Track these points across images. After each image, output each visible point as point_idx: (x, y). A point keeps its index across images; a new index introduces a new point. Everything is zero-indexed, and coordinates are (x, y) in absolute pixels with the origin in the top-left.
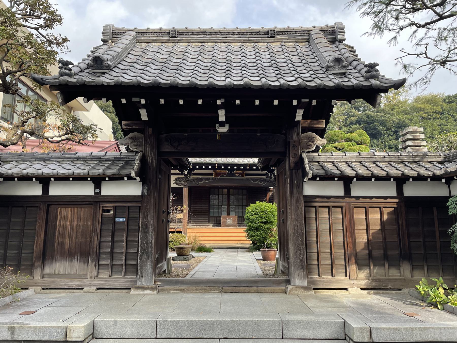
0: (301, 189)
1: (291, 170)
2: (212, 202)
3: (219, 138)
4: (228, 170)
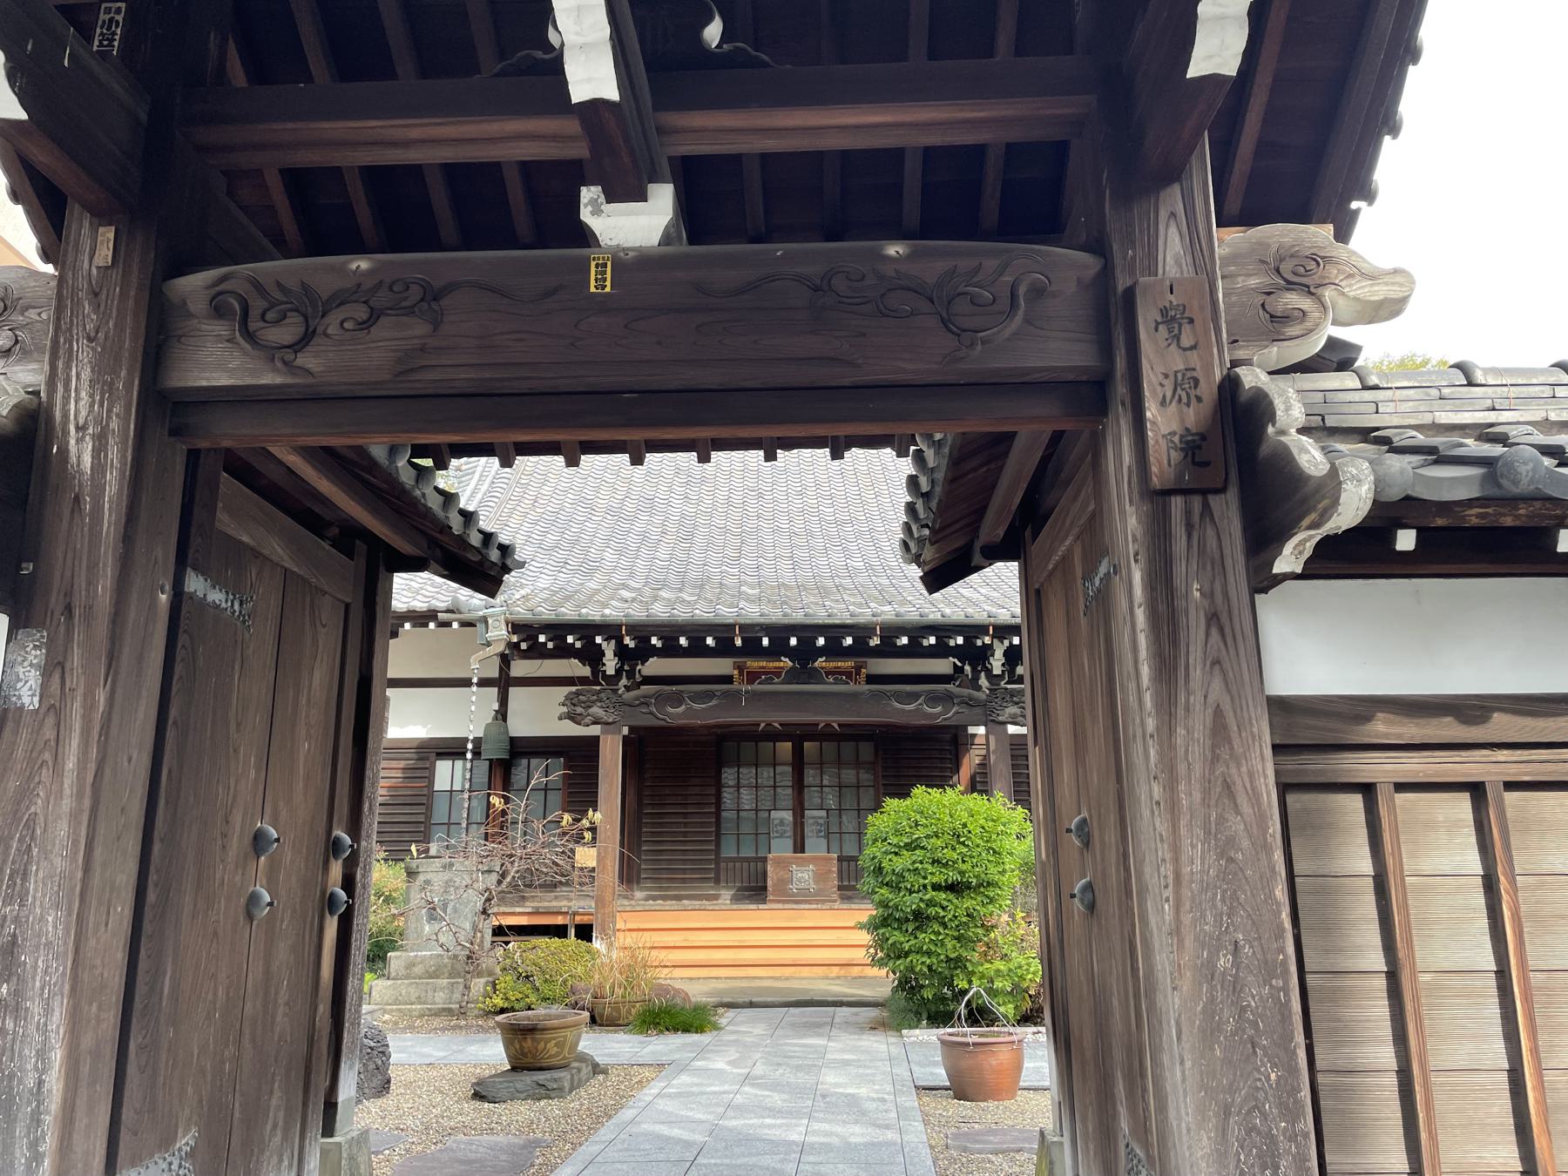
0: (1239, 644)
1: (1156, 498)
2: (728, 796)
3: (599, 282)
4: (791, 653)
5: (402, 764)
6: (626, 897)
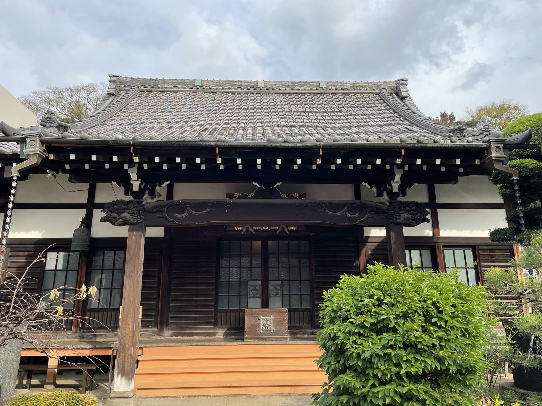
5: (26, 254)
6: (159, 335)
